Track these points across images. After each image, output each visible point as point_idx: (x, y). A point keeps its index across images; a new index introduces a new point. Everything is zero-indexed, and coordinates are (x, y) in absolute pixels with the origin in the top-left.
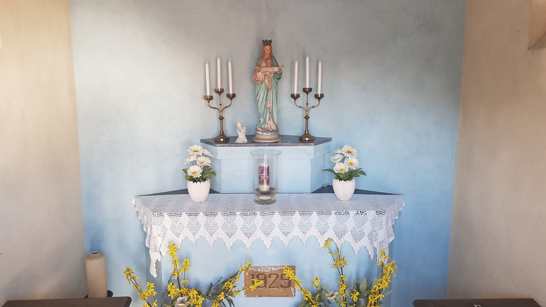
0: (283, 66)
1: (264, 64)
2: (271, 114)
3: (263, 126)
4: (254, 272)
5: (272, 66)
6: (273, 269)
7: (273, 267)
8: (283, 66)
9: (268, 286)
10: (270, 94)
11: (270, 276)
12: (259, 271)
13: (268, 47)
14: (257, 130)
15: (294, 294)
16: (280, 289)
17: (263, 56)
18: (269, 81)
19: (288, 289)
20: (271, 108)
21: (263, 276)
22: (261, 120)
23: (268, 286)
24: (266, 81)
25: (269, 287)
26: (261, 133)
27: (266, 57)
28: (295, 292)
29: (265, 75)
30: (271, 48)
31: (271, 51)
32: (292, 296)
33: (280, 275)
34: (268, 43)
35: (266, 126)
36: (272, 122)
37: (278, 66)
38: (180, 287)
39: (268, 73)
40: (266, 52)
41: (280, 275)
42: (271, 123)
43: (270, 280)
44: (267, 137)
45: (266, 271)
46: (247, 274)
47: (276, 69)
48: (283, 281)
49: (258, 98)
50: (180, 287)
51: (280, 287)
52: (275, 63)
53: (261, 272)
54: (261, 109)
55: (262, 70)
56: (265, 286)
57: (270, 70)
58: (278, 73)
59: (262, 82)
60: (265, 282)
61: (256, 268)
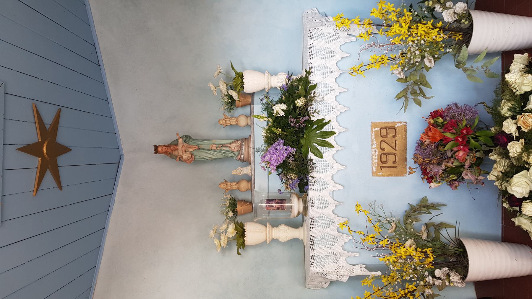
0: (177, 134)
1: (176, 153)
2: (223, 145)
3: (236, 154)
4: (378, 166)
5: (177, 145)
6: (375, 145)
7: (372, 146)
8: (177, 134)
9: (394, 151)
10: (203, 146)
11: (383, 149)
12: (376, 161)
13: (160, 149)
14: (240, 160)
15: (403, 124)
16: (398, 137)
17: (170, 154)
18: (191, 148)
19: (397, 130)
20: (218, 146)
21: (382, 156)
22: (230, 155)
23: (394, 151)
24: (191, 150)
25: (396, 150)
26: (242, 156)
27: (170, 151)
28: (401, 122)
29: (185, 151)
30: (161, 146)
31: (165, 146)
32: (406, 125)
33: (381, 139)
34: (156, 147)
35: (236, 151)
36: (233, 145)
37: (177, 140)
38: (380, 25)
39: (183, 149)
40: (164, 150)
41: (381, 139)
42: (233, 146)
43: (388, 149)
44: (246, 149)
45: (377, 153)
46: (381, 174)
47: (180, 141)
48: (389, 136)
49: (208, 159)
50: (380, 25)
51: (396, 138)
52: (176, 143)
53: (378, 159)
54: (219, 155)
55: (181, 154)
56: (394, 154)
57: (180, 146)
58: (184, 139)
59: (192, 154)
60: (390, 154)
61: (373, 164)
